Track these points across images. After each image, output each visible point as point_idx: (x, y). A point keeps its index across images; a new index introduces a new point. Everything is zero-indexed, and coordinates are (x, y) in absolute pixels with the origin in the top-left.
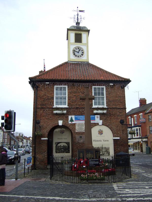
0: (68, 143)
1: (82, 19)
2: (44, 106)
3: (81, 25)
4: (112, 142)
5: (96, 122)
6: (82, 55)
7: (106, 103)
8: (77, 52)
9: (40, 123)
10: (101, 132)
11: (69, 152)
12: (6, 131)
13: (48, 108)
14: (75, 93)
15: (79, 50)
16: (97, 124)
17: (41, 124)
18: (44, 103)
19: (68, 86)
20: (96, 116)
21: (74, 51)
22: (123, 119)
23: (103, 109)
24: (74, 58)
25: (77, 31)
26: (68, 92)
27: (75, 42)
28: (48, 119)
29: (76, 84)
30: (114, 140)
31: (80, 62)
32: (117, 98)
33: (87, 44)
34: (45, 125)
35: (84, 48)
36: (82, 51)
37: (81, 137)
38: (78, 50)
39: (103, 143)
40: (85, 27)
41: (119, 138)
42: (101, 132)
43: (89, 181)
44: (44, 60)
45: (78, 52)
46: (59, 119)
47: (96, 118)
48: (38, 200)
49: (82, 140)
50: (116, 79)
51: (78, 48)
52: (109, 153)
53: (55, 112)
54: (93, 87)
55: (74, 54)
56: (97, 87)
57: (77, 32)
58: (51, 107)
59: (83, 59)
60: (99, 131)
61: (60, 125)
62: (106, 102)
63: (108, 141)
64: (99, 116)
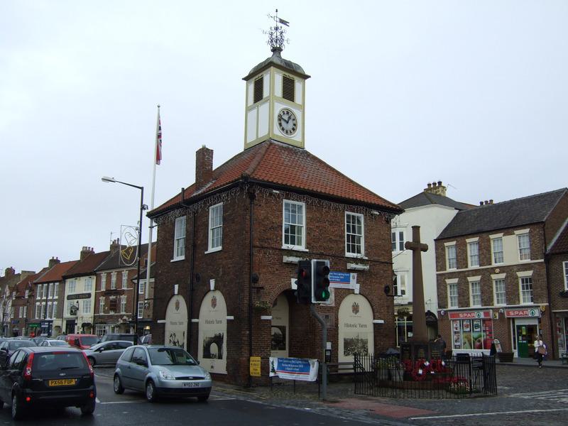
0: (282, 328)
1: (285, 43)
2: (266, 242)
3: (286, 55)
4: (370, 329)
5: (350, 286)
6: (295, 125)
7: (365, 250)
8: (285, 120)
9: (257, 280)
10: (356, 309)
11: (284, 349)
12: (315, 302)
13: (273, 248)
14: (318, 222)
15: (290, 118)
16: (351, 291)
17: (261, 283)
18: (266, 237)
19: (366, 215)
20: (352, 274)
21: (280, 118)
22: (388, 284)
23: (361, 261)
24: (280, 134)
25: (289, 72)
26: (307, 218)
27: (284, 97)
28: (273, 273)
29: (325, 203)
30: (375, 324)
31: (290, 147)
32: (380, 242)
33: (302, 107)
34: (267, 287)
35: (298, 113)
36: (294, 120)
37: (327, 317)
38: (286, 117)
39: (358, 330)
40: (299, 67)
41: (382, 322)
42: (356, 309)
43: (473, 395)
44: (159, 107)
45: (287, 122)
46: (292, 275)
47: (351, 278)
48: (462, 421)
49: (328, 324)
50: (383, 204)
51: (288, 113)
52: (367, 351)
53: (287, 259)
54: (346, 213)
55: (280, 124)
56: (291, 202)
57: (287, 74)
58: (277, 246)
59: (295, 138)
60: (353, 306)
61: (293, 288)
62: (365, 247)
63: (366, 326)
64: (355, 275)
